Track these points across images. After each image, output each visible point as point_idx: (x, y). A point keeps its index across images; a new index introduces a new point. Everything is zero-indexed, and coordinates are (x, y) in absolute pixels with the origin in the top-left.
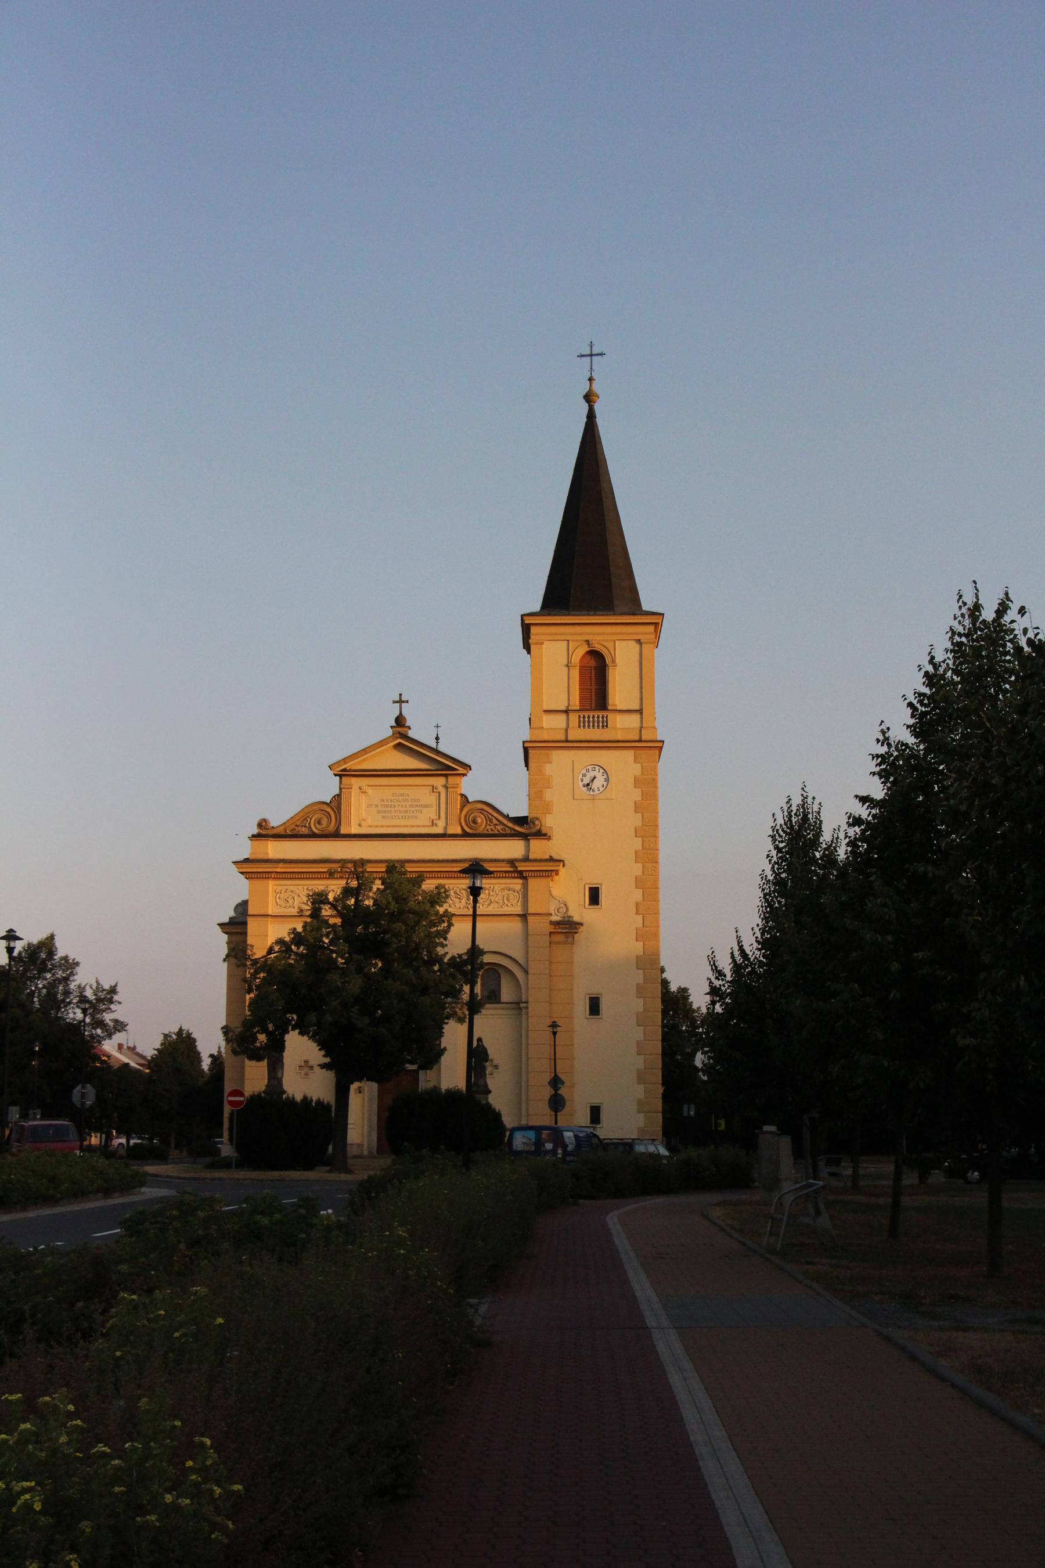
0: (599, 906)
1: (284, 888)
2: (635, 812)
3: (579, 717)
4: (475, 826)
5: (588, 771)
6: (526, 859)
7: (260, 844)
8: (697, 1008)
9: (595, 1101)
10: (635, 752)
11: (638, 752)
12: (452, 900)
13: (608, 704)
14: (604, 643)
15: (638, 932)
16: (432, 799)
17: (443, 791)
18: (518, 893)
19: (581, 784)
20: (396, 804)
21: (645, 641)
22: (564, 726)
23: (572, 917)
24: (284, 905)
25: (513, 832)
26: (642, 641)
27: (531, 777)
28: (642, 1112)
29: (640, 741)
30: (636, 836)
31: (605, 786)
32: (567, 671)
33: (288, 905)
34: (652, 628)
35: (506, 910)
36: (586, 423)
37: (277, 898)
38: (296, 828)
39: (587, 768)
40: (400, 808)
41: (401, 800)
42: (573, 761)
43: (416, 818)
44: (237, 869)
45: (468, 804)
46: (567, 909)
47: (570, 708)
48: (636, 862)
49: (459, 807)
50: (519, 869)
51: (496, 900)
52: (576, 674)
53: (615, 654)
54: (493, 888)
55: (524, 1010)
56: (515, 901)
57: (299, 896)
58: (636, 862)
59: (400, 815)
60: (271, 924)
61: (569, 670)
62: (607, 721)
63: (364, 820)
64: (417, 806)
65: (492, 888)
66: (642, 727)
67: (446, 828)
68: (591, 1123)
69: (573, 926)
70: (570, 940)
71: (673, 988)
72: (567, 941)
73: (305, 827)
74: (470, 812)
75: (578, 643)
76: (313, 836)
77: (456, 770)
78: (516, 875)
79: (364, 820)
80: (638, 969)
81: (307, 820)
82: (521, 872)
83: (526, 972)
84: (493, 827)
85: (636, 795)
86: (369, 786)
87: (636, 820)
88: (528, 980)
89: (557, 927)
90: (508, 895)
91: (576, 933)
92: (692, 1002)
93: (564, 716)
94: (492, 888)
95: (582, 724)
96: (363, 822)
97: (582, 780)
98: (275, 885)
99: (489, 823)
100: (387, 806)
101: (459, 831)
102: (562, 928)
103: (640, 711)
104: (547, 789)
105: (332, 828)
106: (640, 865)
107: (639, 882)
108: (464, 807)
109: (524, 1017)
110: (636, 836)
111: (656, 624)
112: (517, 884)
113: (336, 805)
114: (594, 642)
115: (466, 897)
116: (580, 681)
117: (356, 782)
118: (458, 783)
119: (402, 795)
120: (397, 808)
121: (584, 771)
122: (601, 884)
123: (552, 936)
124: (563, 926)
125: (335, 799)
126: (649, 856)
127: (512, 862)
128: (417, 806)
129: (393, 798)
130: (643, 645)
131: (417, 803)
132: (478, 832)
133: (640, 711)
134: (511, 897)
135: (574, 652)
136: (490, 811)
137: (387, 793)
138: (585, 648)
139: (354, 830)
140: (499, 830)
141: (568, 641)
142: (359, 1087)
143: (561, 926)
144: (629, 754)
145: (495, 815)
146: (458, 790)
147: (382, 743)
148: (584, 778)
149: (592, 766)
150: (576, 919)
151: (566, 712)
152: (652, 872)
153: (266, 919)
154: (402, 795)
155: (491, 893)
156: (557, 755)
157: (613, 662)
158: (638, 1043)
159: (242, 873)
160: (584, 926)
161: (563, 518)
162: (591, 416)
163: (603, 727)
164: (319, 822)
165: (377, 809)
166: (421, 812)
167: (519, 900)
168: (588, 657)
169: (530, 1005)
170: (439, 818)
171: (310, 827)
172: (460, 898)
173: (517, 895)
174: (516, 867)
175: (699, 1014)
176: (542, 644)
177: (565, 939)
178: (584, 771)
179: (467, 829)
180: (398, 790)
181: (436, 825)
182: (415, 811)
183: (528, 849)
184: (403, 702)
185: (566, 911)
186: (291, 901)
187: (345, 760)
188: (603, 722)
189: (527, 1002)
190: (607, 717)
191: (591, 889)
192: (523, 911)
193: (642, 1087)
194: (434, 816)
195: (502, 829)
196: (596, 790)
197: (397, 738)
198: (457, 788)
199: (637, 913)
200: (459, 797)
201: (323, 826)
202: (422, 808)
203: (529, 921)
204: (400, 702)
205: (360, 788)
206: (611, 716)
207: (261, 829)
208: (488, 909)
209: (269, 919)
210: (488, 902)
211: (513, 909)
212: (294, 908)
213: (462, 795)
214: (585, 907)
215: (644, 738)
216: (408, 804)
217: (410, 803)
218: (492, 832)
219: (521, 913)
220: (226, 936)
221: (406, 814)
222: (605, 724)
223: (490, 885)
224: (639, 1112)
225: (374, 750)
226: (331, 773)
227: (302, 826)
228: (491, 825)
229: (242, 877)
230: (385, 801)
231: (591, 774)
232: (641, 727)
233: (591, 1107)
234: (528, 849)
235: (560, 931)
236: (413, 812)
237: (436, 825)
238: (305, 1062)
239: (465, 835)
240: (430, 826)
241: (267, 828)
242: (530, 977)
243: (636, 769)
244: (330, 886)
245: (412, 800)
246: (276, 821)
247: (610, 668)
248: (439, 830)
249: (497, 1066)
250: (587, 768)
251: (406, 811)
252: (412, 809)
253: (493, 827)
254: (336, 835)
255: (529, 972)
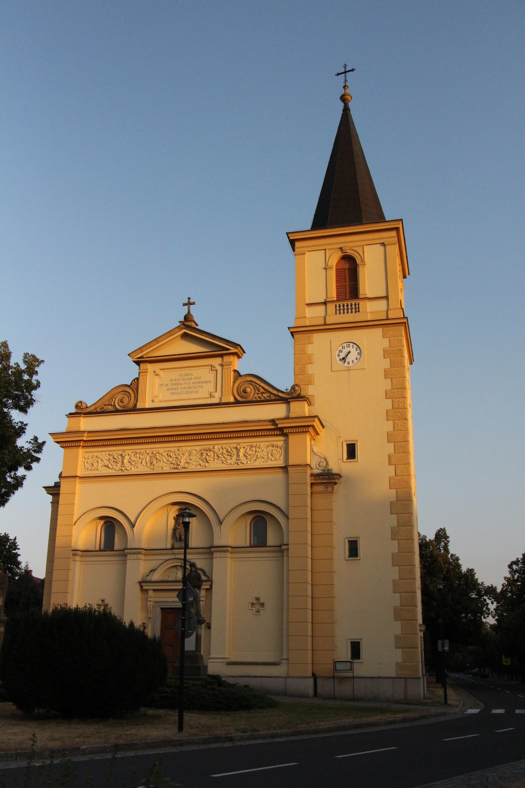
0: (356, 460)
1: (91, 455)
2: (385, 378)
3: (336, 306)
4: (245, 395)
5: (343, 348)
6: (287, 418)
7: (74, 420)
8: (481, 583)
9: (355, 637)
10: (383, 330)
11: (387, 329)
12: (225, 458)
13: (359, 294)
14: (354, 249)
15: (392, 481)
16: (211, 376)
17: (219, 368)
18: (281, 448)
19: (338, 359)
20: (182, 382)
21: (388, 243)
22: (323, 314)
23: (332, 470)
24: (90, 468)
25: (277, 398)
26: (385, 243)
27: (296, 356)
28: (400, 648)
29: (387, 319)
30: (386, 398)
31: (358, 358)
32: (325, 272)
33: (93, 468)
34: (394, 233)
35: (270, 464)
36: (343, 114)
37: (85, 463)
38: (104, 407)
39: (343, 345)
40: (185, 386)
41: (186, 379)
42: (331, 341)
43: (197, 392)
44: (53, 439)
45: (239, 378)
46: (327, 463)
47: (328, 300)
48: (387, 420)
49: (232, 380)
50: (279, 426)
51: (262, 455)
52: (333, 274)
53: (364, 255)
54: (260, 446)
55: (285, 552)
56: (278, 456)
57: (102, 460)
58: (387, 420)
59: (185, 390)
60: (79, 484)
61: (326, 271)
62: (359, 308)
63: (156, 397)
64: (199, 382)
65: (258, 445)
66: (389, 309)
67: (221, 398)
68: (351, 659)
69: (332, 476)
70: (330, 489)
71: (29, 569)
72: (327, 490)
73: (111, 405)
74: (241, 384)
75: (332, 251)
76: (116, 411)
77: (228, 349)
78: (278, 433)
79: (156, 397)
80: (391, 513)
81: (113, 400)
82: (281, 429)
83: (287, 517)
84: (260, 395)
85: (386, 363)
86: (161, 369)
87: (387, 384)
88: (288, 523)
89: (317, 478)
90: (272, 450)
91: (336, 483)
92: (477, 579)
93: (323, 307)
94: (258, 445)
95: (339, 311)
96: (156, 398)
97: (339, 355)
98: (85, 452)
99: (257, 392)
100: (175, 384)
101: (232, 400)
102: (323, 479)
103: (387, 298)
104: (309, 365)
105: (131, 405)
106: (391, 422)
107: (390, 438)
108: (236, 381)
109: (285, 558)
110: (386, 398)
111: (397, 229)
112: (280, 441)
113: (135, 387)
114: (346, 248)
115: (236, 454)
116: (337, 280)
117: (150, 367)
118: (232, 361)
119: (187, 375)
120: (183, 386)
121: (340, 348)
122: (357, 441)
123: (313, 487)
124: (323, 477)
125: (135, 382)
126: (399, 414)
127: (273, 421)
128: (199, 382)
129: (180, 378)
130: (386, 246)
131: (199, 380)
132: (249, 399)
133: (387, 298)
134: (275, 452)
135: (329, 258)
136: (258, 382)
137: (175, 375)
138: (339, 254)
139: (147, 406)
140: (266, 397)
141: (325, 250)
142: (143, 623)
143: (321, 477)
144: (378, 332)
145: (262, 384)
146: (231, 366)
147: (170, 333)
148: (340, 354)
149: (347, 344)
150: (335, 471)
151: (325, 303)
152: (401, 428)
153: (74, 480)
154: (187, 375)
155: (258, 450)
156: (316, 337)
157: (362, 262)
158: (394, 582)
159: (58, 442)
160: (342, 477)
161: (326, 176)
162: (346, 110)
163: (355, 312)
164: (122, 401)
165: (167, 387)
166: (202, 387)
167: (281, 455)
168: (343, 262)
169: (290, 546)
170: (216, 391)
171: (115, 405)
172: (231, 456)
173: (280, 450)
174: (277, 425)
175: (483, 587)
176: (304, 254)
177: (325, 489)
178: (340, 348)
179: (238, 398)
180: (184, 372)
181: (213, 397)
182: (197, 387)
183: (289, 410)
184: (191, 304)
185: (326, 465)
186: (95, 464)
187: (141, 349)
188: (355, 309)
189: (287, 545)
190: (358, 305)
191: (348, 445)
192: (285, 464)
193: (399, 623)
194: (212, 390)
195: (268, 397)
196: (351, 362)
197: (183, 328)
198: (230, 365)
199: (390, 464)
200: (232, 373)
201: (126, 403)
202: (202, 384)
203: (289, 472)
204: (189, 304)
205: (154, 372)
206: (362, 303)
207: (77, 409)
208: (254, 464)
209: (78, 480)
210: (255, 457)
211: (276, 462)
212: (98, 470)
213: (235, 371)
214: (343, 462)
215: (390, 317)
216: (191, 382)
217: (193, 381)
218: (259, 399)
219: (283, 465)
220: (51, 497)
221: (190, 390)
222: (357, 310)
223: (257, 443)
224: (397, 648)
225: (165, 339)
226: (130, 360)
227: (109, 405)
228: (258, 394)
229: (58, 445)
230: (174, 381)
231: (346, 350)
232: (388, 309)
233: (351, 642)
234: (289, 410)
235: (320, 481)
236: (196, 387)
237: (213, 397)
238: (102, 600)
239: (237, 403)
240: (208, 398)
241: (82, 407)
242: (290, 521)
243: (385, 343)
244: (127, 451)
245: (195, 378)
246: (90, 401)
247: (360, 266)
248: (216, 400)
249: (263, 604)
250: (343, 345)
251: (190, 388)
252: (195, 385)
253: (260, 395)
254: (134, 410)
255: (290, 517)
